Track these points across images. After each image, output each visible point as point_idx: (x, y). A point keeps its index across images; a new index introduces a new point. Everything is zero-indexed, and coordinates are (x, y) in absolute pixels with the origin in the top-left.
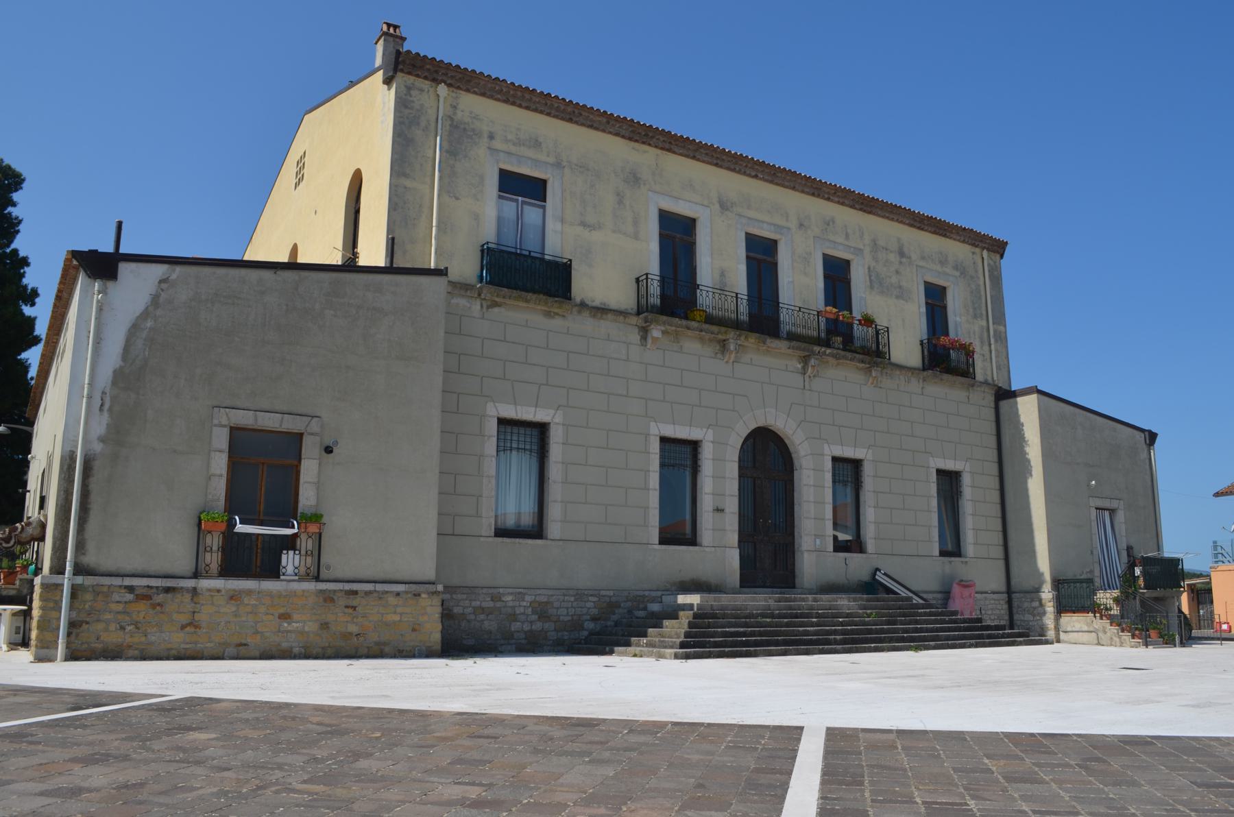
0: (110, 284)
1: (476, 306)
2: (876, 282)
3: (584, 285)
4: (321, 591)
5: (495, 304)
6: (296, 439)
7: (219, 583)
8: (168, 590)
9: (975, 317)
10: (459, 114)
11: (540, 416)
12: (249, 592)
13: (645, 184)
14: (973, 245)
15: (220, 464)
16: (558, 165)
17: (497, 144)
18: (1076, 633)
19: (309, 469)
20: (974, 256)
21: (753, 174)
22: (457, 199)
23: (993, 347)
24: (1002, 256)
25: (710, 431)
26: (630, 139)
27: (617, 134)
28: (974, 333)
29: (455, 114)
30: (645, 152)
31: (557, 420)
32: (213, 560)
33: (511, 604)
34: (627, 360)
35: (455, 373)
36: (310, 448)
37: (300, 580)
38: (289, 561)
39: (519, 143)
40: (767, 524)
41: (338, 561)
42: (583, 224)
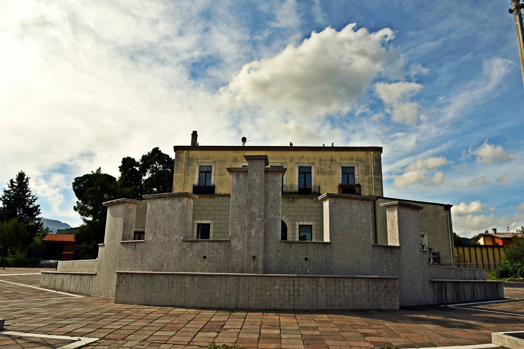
2: (320, 172)
3: (218, 191)
9: (366, 174)
10: (190, 156)
11: (310, 223)
13: (238, 161)
14: (366, 151)
16: (215, 162)
17: (199, 161)
18: (32, 348)
20: (367, 154)
21: (273, 150)
22: (189, 175)
23: (373, 183)
25: (314, 222)
28: (365, 180)
29: (189, 156)
30: (239, 152)
31: (212, 223)
34: (210, 206)
35: (198, 215)
39: (204, 159)
42: (221, 175)
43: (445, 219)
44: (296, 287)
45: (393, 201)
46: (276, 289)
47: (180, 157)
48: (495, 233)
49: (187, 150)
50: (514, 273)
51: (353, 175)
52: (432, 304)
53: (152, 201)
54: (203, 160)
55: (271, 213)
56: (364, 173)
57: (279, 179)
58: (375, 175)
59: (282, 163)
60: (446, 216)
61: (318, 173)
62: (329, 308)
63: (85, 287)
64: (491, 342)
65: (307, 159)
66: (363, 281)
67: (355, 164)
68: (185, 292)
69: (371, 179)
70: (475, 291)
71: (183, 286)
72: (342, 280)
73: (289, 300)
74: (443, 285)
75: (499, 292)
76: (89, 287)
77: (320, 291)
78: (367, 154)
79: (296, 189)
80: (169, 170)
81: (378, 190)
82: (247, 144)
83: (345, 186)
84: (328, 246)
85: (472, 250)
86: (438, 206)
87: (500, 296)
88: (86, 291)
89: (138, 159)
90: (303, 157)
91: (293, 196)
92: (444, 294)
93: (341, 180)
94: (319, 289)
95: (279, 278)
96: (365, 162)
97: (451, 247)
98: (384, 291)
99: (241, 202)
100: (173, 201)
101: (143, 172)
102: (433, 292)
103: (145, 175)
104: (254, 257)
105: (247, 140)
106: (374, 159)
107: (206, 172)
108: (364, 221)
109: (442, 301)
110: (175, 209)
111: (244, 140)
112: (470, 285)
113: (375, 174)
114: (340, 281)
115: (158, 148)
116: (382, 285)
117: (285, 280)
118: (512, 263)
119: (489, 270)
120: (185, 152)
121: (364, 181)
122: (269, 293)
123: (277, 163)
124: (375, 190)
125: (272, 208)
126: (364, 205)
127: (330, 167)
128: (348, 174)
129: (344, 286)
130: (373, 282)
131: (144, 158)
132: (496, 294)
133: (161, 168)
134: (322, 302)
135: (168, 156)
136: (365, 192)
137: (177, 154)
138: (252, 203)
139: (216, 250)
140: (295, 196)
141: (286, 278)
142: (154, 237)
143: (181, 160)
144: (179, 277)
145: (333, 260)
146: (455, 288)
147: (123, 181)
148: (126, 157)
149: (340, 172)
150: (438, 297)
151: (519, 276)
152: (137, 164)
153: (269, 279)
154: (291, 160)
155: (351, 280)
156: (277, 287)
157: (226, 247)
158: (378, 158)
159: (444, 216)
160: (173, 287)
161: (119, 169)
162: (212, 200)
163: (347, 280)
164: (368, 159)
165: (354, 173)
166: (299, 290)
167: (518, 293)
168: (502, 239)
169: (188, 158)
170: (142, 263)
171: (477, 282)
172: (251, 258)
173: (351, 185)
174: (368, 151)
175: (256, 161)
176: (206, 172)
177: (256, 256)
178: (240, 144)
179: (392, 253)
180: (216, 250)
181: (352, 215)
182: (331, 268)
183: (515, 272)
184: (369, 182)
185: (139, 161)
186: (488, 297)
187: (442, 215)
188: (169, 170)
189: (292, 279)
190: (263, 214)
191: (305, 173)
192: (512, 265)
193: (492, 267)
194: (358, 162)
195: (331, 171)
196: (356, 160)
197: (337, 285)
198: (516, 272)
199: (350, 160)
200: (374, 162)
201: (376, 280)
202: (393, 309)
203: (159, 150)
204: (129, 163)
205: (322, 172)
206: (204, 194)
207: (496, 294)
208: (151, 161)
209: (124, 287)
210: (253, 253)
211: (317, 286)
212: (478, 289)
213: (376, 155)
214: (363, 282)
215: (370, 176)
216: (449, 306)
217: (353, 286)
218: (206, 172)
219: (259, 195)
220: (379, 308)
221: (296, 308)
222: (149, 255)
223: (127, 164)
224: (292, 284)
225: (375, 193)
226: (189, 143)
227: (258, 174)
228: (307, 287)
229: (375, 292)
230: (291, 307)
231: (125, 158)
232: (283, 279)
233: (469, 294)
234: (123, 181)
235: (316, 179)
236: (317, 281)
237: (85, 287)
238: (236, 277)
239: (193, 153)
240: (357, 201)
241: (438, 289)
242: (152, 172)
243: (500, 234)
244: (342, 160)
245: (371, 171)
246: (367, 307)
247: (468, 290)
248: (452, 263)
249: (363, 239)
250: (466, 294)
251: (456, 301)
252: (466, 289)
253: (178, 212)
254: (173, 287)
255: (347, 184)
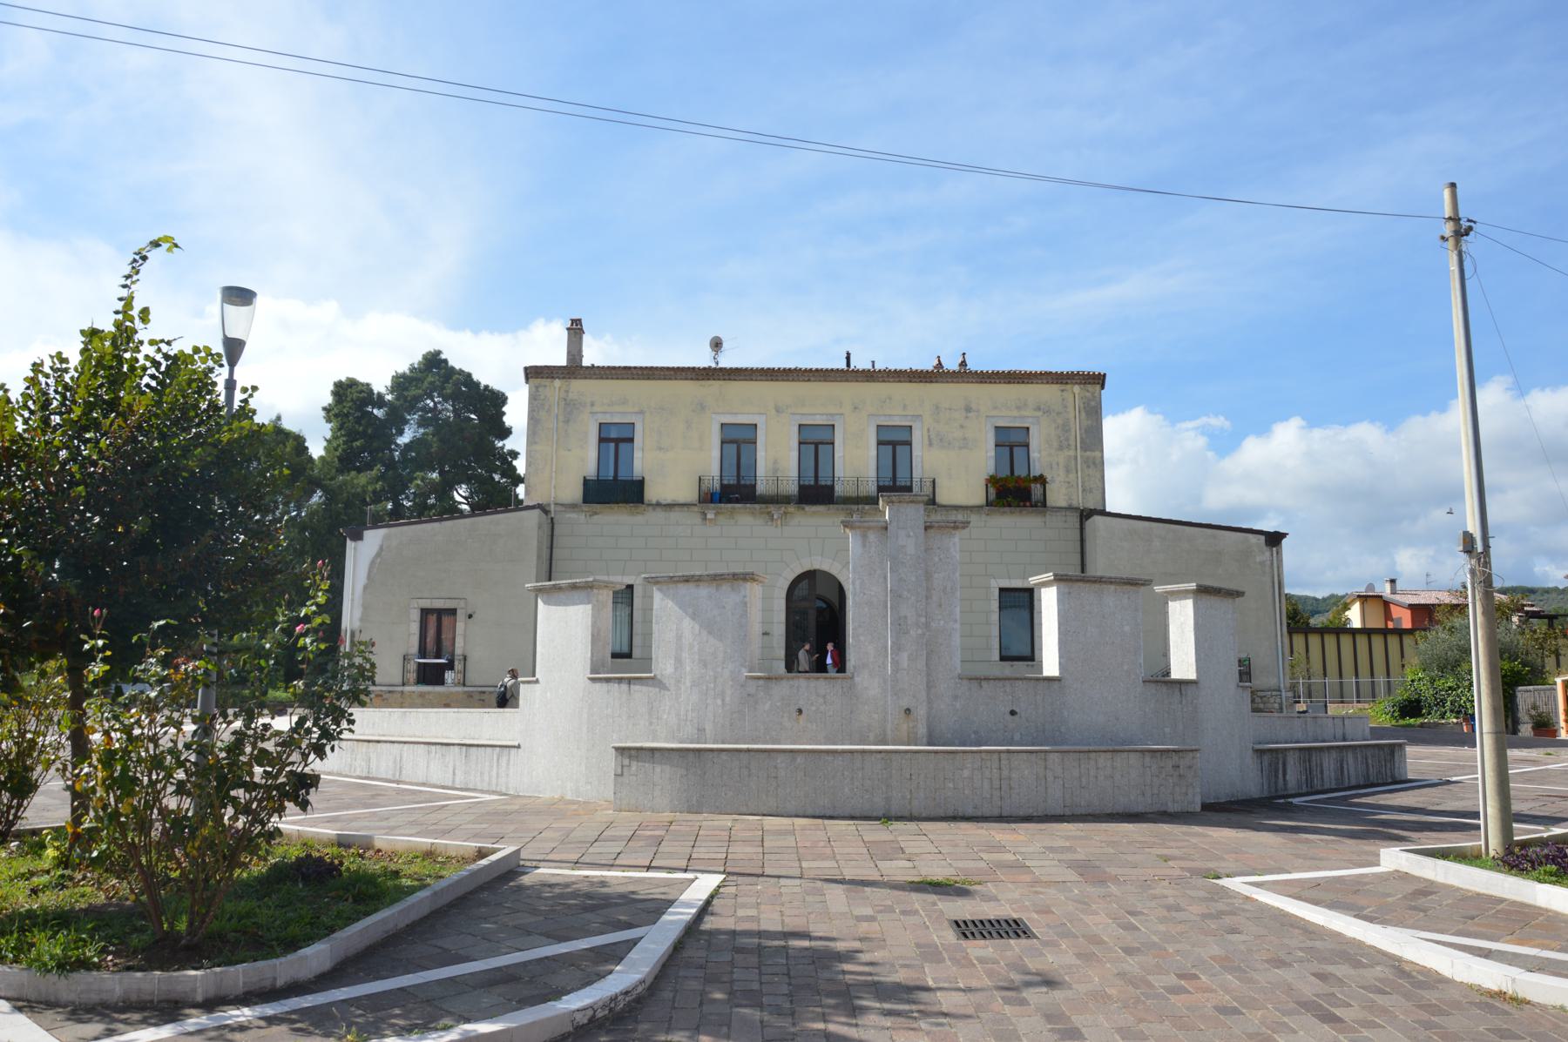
0: (359, 542)
1: (582, 517)
3: (652, 493)
4: (466, 692)
5: (596, 513)
6: (453, 612)
7: (414, 688)
8: (390, 692)
9: (1061, 448)
10: (570, 394)
12: (429, 693)
15: (415, 628)
16: (641, 412)
17: (596, 409)
19: (460, 626)
20: (1064, 393)
23: (1079, 473)
24: (1103, 387)
26: (698, 379)
27: (686, 379)
28: (1058, 464)
32: (412, 676)
33: (341, 663)
36: (461, 615)
37: (456, 685)
38: (449, 676)
40: (65, 619)
41: (472, 677)
42: (660, 449)
43: (1267, 569)
44: (1005, 773)
45: (1397, 843)
46: (965, 776)
47: (542, 397)
48: (1394, 592)
49: (564, 378)
50: (1436, 705)
51: (1025, 448)
52: (1256, 796)
53: (665, 587)
54: (609, 405)
55: (940, 617)
56: (1055, 444)
57: (954, 544)
58: (1085, 451)
59: (832, 415)
60: (1269, 562)
61: (931, 444)
62: (1068, 812)
63: (482, 774)
64: (1379, 865)
65: (900, 404)
66: (1132, 755)
67: (1030, 420)
68: (778, 786)
69: (1073, 462)
70: (1345, 766)
71: (773, 775)
72: (1093, 755)
73: (991, 798)
74: (1280, 756)
75: (1397, 765)
76: (498, 774)
77: (1050, 779)
78: (1063, 391)
79: (792, 488)
80: (473, 416)
81: (1091, 491)
82: (727, 361)
83: (1006, 479)
84: (1056, 685)
85: (1330, 640)
86: (1250, 536)
87: (1397, 775)
88: (489, 784)
89: (381, 383)
90: (890, 399)
91: (863, 508)
92: (1280, 776)
93: (992, 463)
94: (1050, 774)
95: (970, 755)
96: (1058, 413)
97: (1279, 644)
98: (1172, 776)
99: (873, 593)
100: (717, 589)
101: (398, 423)
102: (1259, 773)
103: (401, 433)
104: (908, 711)
105: (724, 345)
106: (1082, 406)
107: (615, 440)
108: (1127, 628)
109: (1276, 790)
110: (724, 607)
111: (717, 344)
112: (1334, 754)
113: (1084, 449)
114: (1089, 759)
115: (439, 352)
116: (1170, 763)
117: (982, 759)
118: (1432, 681)
119: (1374, 696)
120: (557, 383)
121: (1055, 466)
122: (951, 785)
123: (818, 417)
124: (1084, 490)
125: (940, 606)
126: (1126, 596)
127: (962, 427)
128: (1011, 447)
129: (1097, 769)
130: (1152, 757)
131: (401, 383)
132: (1388, 772)
133: (447, 410)
134: (1055, 800)
135: (469, 375)
136: (1057, 495)
137: (534, 389)
138: (900, 596)
139: (824, 697)
140: (867, 507)
141: (983, 755)
142: (676, 669)
143: (546, 408)
144: (763, 756)
145: (1066, 714)
146: (1304, 761)
147: (340, 450)
148: (343, 379)
149: (990, 439)
150: (1269, 784)
151: (1448, 714)
152: (379, 401)
153: (952, 756)
154: (855, 408)
155: (1109, 755)
156: (966, 773)
157: (845, 690)
158: (1093, 403)
159: (1264, 562)
160: (749, 776)
161: (323, 413)
162: (639, 519)
163: (1103, 755)
164: (1066, 407)
165: (1027, 446)
166: (1010, 779)
167: (1439, 765)
168: (1412, 607)
169: (565, 400)
170: (651, 724)
171: (1350, 746)
172: (903, 712)
173: (1019, 477)
174: (1067, 383)
175: (905, 505)
176: (618, 441)
177: (912, 709)
178: (703, 359)
179: (1181, 694)
180: (824, 697)
181: (1104, 617)
182: (1063, 729)
183: (1438, 704)
184: (1068, 471)
185: (383, 390)
186: (1371, 778)
187: (1258, 559)
188: (473, 416)
189: (995, 756)
190: (923, 620)
191: (894, 444)
192: (1432, 683)
193: (1382, 689)
194: (1039, 414)
195: (965, 439)
196: (1035, 410)
197: (1082, 766)
198: (1443, 701)
199: (1018, 408)
200: (1083, 414)
201: (1158, 754)
202: (1190, 810)
203: (443, 356)
204: (355, 396)
205: (941, 440)
206: (614, 503)
207: (1388, 772)
208: (420, 391)
209: (635, 778)
210: (905, 703)
211: (1046, 768)
212: (1351, 761)
213: (1088, 394)
214: (1133, 758)
215: (1072, 453)
216: (1295, 801)
217: (1113, 768)
218: (615, 440)
219: (913, 579)
220: (1162, 809)
221: (1004, 814)
222: (667, 708)
223: (349, 399)
224: (996, 765)
225: (1083, 498)
226: (560, 359)
227: (911, 534)
228: (1026, 772)
229: (1155, 779)
230: (996, 812)
231: (340, 382)
232: (977, 756)
233: (1333, 774)
234: (340, 450)
235: (925, 460)
236: (1045, 760)
237: (482, 774)
238: (883, 755)
239: (578, 386)
240: (1112, 587)
241: (1270, 765)
242: (422, 423)
243: (1404, 593)
244: (995, 408)
245: (1072, 438)
246: (1141, 809)
247: (1329, 764)
248: (1282, 686)
249: (1126, 668)
250: (1326, 773)
251: (1304, 790)
252: (1325, 765)
253: (733, 614)
254: (749, 776)
255: (1009, 473)
